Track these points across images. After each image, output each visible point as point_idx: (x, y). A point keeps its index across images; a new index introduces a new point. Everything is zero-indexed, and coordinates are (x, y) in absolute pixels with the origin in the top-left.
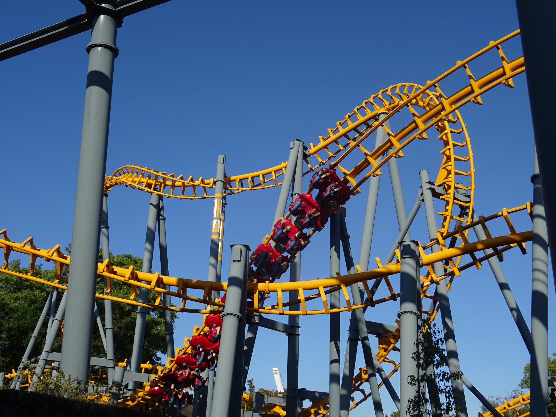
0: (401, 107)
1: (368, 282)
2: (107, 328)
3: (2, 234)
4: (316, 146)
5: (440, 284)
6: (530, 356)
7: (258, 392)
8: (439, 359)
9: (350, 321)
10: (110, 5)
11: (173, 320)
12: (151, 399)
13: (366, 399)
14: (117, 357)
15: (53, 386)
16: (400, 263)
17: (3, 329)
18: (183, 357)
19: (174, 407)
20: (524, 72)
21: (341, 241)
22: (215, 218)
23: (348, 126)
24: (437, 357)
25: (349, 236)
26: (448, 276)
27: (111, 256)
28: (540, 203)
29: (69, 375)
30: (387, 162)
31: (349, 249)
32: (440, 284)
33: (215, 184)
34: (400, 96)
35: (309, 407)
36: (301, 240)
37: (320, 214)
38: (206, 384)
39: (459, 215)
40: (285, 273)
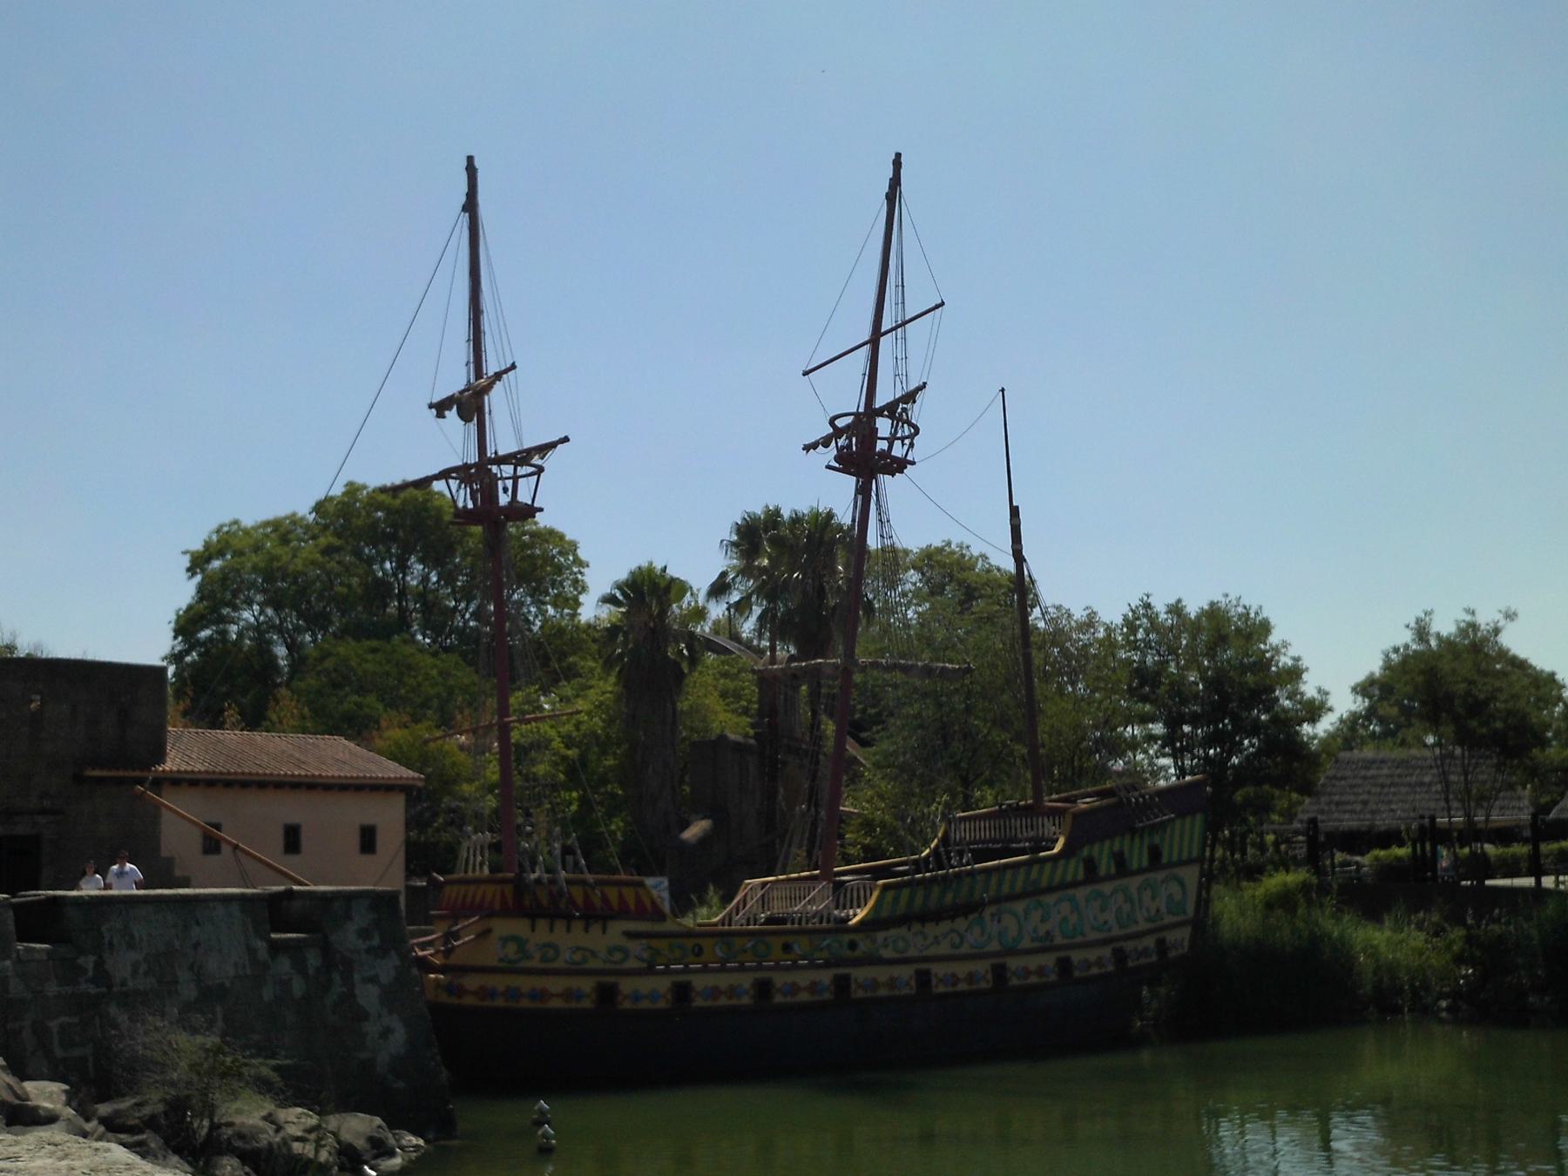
0: (497, 302)
1: (511, 481)
3: (886, 442)
7: (1036, 602)
8: (378, 1121)
9: (940, 924)
10: (44, 656)
13: (901, 163)
17: (571, 558)
18: (860, 613)
19: (502, 507)
20: (910, 317)
21: (1488, 882)
22: (1538, 882)
23: (1113, 950)
26: (874, 481)
28: (1064, 834)
30: (907, 319)
31: (1531, 852)
36: (1495, 705)
38: (873, 542)
40: (441, 469)
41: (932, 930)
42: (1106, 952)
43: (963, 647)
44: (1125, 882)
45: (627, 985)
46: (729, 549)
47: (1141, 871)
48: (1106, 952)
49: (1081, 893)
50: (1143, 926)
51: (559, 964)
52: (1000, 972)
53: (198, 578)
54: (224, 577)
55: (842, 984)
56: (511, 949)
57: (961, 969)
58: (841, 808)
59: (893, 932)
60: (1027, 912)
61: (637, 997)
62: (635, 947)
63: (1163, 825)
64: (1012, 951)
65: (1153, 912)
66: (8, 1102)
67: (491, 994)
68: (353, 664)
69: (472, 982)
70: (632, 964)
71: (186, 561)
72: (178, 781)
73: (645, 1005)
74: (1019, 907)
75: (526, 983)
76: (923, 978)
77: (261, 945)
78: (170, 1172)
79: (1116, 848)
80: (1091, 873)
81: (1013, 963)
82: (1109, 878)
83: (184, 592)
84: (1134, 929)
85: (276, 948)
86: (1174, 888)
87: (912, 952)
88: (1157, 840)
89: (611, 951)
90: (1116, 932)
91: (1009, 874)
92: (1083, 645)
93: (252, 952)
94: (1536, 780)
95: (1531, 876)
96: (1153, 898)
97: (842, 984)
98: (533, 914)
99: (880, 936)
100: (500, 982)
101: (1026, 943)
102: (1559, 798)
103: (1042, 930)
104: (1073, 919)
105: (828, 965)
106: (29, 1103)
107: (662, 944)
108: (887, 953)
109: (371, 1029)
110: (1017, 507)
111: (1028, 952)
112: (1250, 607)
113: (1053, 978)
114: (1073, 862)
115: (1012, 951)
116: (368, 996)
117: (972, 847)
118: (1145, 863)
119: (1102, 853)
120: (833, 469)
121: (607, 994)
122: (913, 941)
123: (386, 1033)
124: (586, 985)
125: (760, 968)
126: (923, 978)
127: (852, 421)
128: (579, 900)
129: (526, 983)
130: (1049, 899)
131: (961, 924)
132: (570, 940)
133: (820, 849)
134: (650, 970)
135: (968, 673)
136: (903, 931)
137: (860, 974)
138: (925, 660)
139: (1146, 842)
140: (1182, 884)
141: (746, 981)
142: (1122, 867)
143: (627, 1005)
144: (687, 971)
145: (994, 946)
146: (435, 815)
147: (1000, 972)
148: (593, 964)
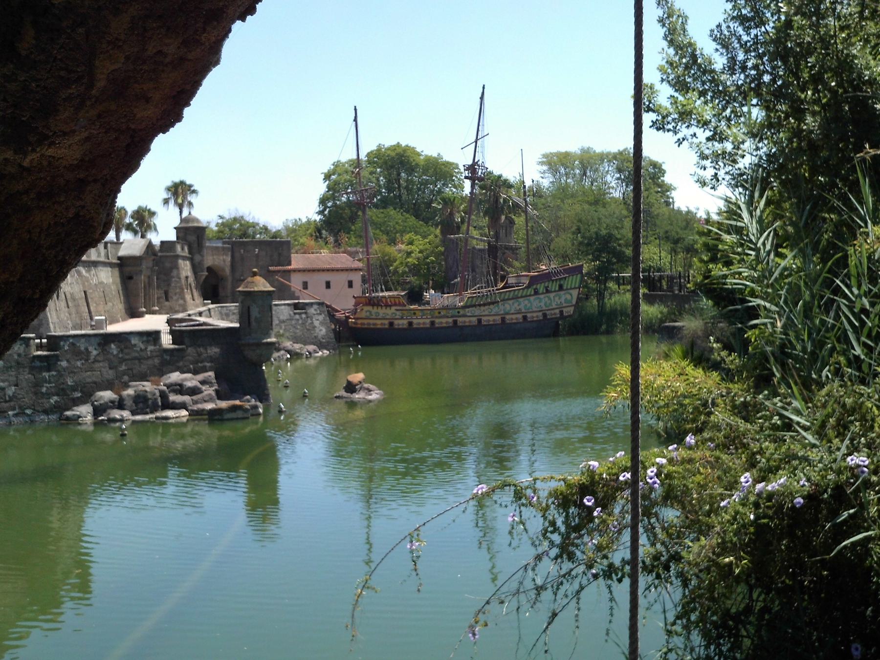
2: (295, 271)
5: (398, 143)
6: (124, 187)
11: (671, 43)
13: (179, 118)
14: (816, 159)
15: (748, 145)
16: (745, 257)
24: (783, 40)
25: (243, 20)
27: (137, 362)
29: (24, 646)
32: (398, 143)
33: (683, 596)
34: (336, 397)
37: (239, 327)
39: (164, 132)
41: (482, 308)
42: (540, 314)
44: (548, 295)
45: (396, 322)
47: (555, 291)
48: (540, 314)
49: (532, 298)
50: (554, 306)
51: (380, 317)
52: (503, 319)
53: (327, 182)
54: (336, 183)
55: (455, 322)
56: (368, 314)
57: (491, 318)
58: (237, 304)
59: (471, 309)
60: (513, 304)
61: (399, 325)
62: (398, 313)
63: (565, 278)
64: (508, 314)
65: (559, 303)
67: (364, 324)
69: (359, 322)
70: (397, 317)
71: (323, 176)
73: (401, 327)
74: (511, 302)
75: (371, 322)
76: (480, 321)
77: (291, 313)
79: (546, 285)
80: (536, 293)
81: (508, 317)
82: (543, 293)
83: (321, 188)
84: (551, 307)
85: (295, 314)
86: (569, 297)
87: (476, 314)
88: (562, 282)
89: (392, 314)
90: (544, 308)
91: (508, 293)
93: (290, 315)
96: (559, 299)
97: (455, 322)
98: (373, 305)
99: (467, 310)
100: (366, 321)
101: (512, 311)
103: (518, 308)
104: (529, 305)
105: (452, 317)
107: (405, 312)
108: (468, 314)
109: (317, 330)
111: (513, 314)
113: (521, 321)
114: (530, 290)
115: (508, 314)
116: (317, 323)
118: (557, 289)
119: (541, 288)
121: (391, 324)
122: (477, 311)
123: (321, 330)
124: (386, 322)
125: (432, 318)
126: (480, 321)
128: (384, 301)
129: (371, 322)
130: (521, 300)
131: (492, 307)
132: (382, 311)
134: (402, 318)
136: (474, 308)
137: (460, 320)
139: (558, 283)
140: (571, 295)
141: (428, 321)
142: (548, 291)
143: (396, 327)
144: (412, 318)
145: (502, 312)
147: (503, 319)
148: (388, 317)
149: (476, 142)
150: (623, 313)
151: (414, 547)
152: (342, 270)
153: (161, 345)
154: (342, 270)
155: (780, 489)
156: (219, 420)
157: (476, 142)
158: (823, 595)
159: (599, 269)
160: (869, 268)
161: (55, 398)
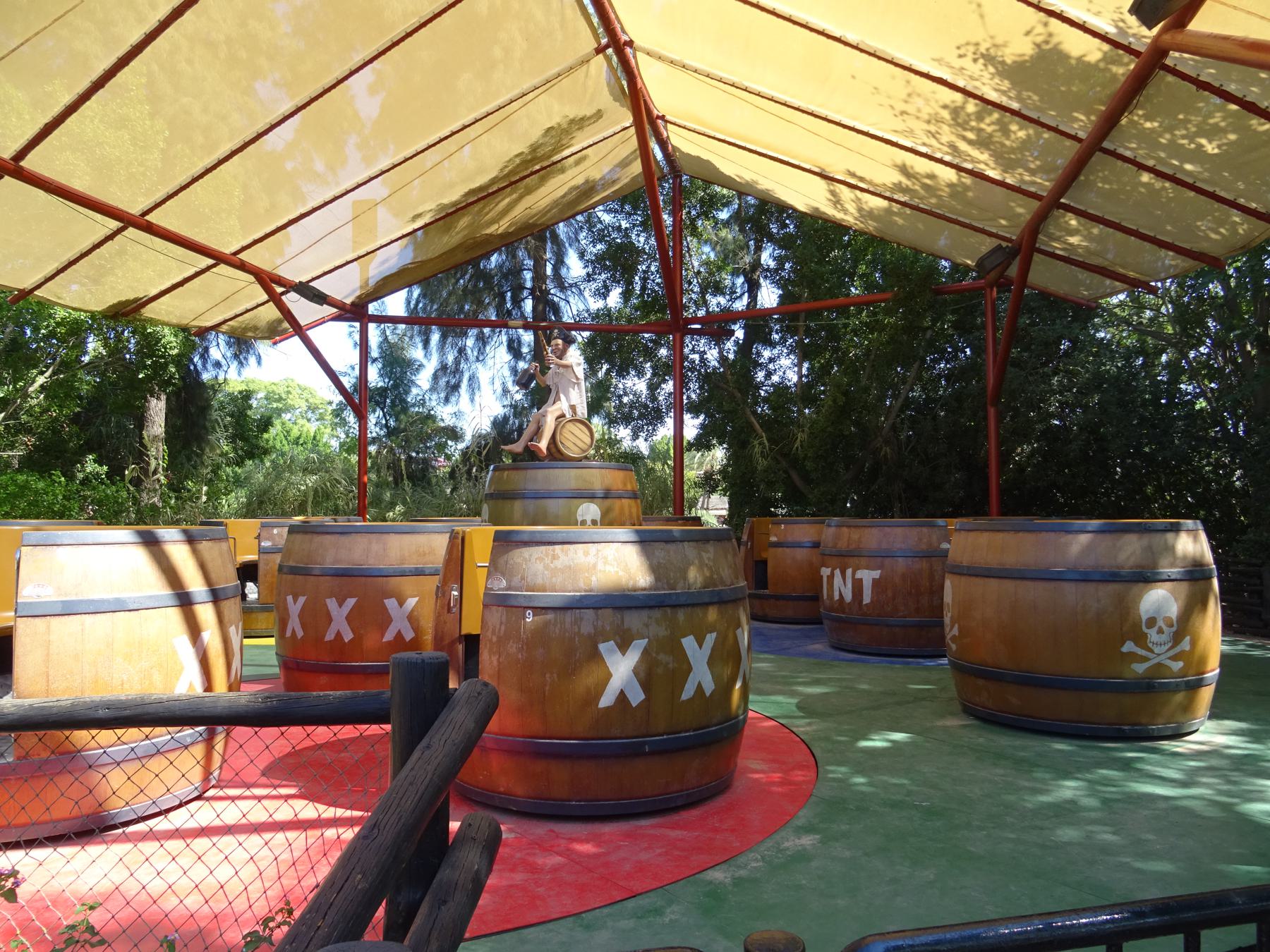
4: (601, 525)
12: (1238, 139)
35: (1136, 169)
43: (558, 860)
46: (1004, 244)
66: (637, 662)
68: (465, 476)
72: (1173, 71)
78: (978, 149)
92: (88, 403)
94: (806, 365)
95: (1199, 936)
102: (44, 369)
106: (1025, 238)
110: (861, 580)
112: (24, 880)
117: (157, 409)
120: (935, 216)
127: (251, 581)
133: (293, 530)
135: (429, 418)
138: (1020, 174)
146: (1189, 469)
149: (661, 887)
150: (243, 926)
151: (1233, 283)
152: (660, 58)
153: (1255, 945)
154: (660, 58)
155: (1093, 246)
156: (725, 788)
157: (661, 887)
158: (848, 505)
159: (137, 350)
160: (797, 448)
161: (1249, 347)
